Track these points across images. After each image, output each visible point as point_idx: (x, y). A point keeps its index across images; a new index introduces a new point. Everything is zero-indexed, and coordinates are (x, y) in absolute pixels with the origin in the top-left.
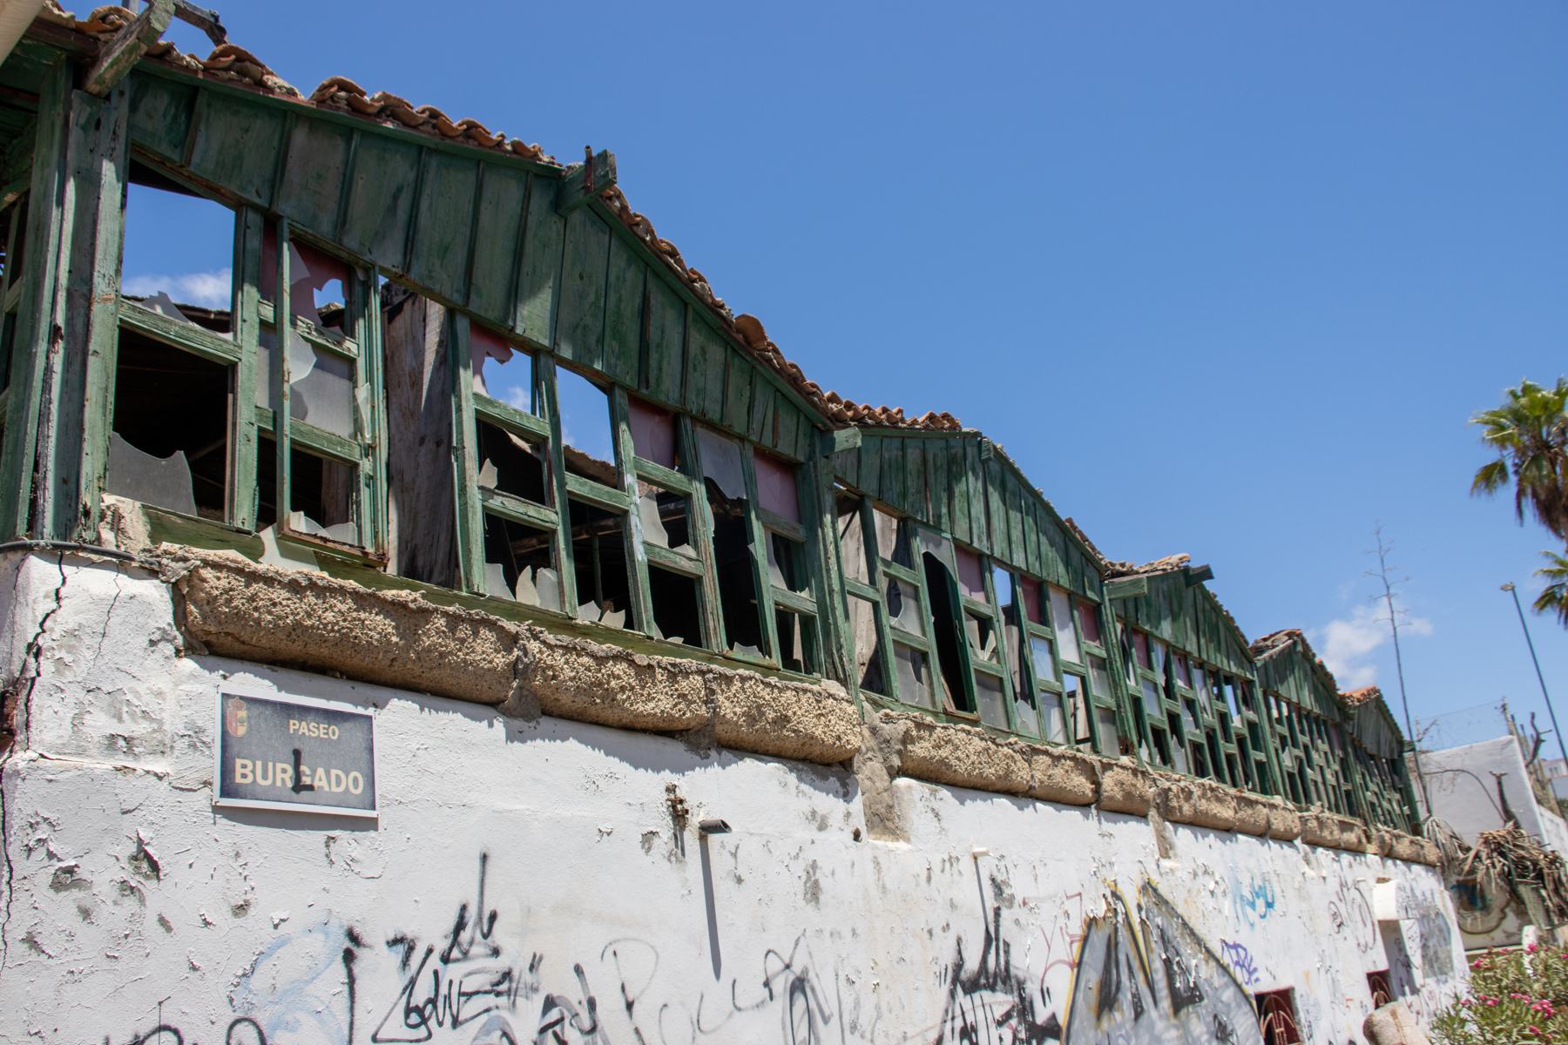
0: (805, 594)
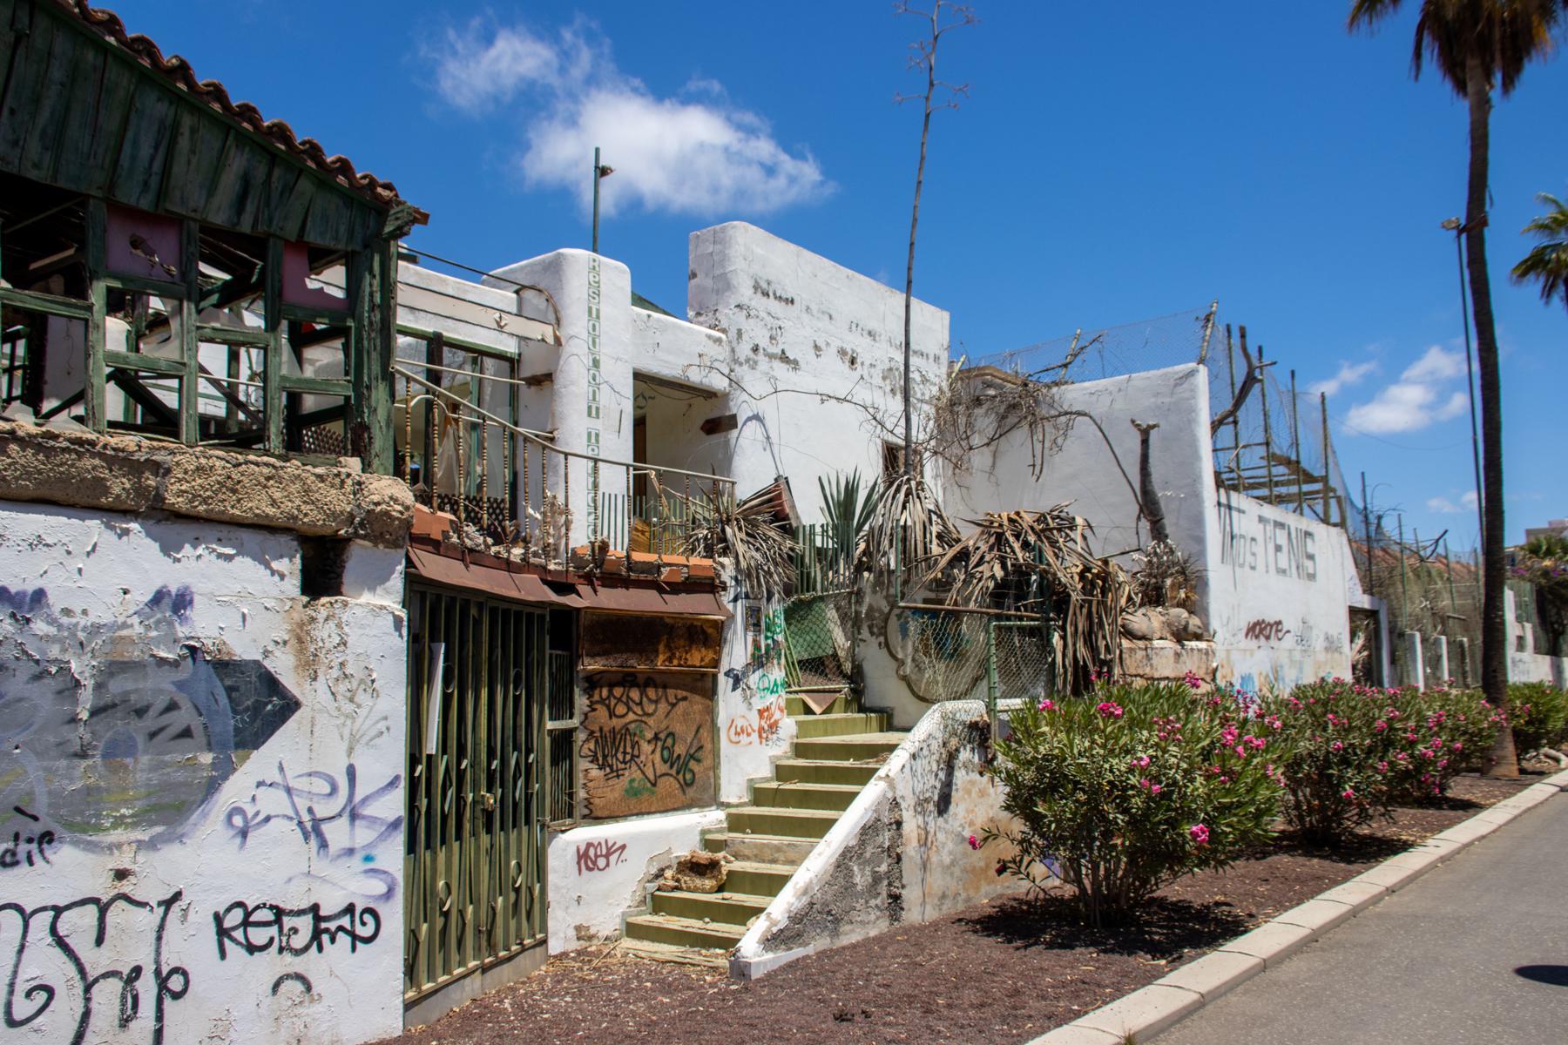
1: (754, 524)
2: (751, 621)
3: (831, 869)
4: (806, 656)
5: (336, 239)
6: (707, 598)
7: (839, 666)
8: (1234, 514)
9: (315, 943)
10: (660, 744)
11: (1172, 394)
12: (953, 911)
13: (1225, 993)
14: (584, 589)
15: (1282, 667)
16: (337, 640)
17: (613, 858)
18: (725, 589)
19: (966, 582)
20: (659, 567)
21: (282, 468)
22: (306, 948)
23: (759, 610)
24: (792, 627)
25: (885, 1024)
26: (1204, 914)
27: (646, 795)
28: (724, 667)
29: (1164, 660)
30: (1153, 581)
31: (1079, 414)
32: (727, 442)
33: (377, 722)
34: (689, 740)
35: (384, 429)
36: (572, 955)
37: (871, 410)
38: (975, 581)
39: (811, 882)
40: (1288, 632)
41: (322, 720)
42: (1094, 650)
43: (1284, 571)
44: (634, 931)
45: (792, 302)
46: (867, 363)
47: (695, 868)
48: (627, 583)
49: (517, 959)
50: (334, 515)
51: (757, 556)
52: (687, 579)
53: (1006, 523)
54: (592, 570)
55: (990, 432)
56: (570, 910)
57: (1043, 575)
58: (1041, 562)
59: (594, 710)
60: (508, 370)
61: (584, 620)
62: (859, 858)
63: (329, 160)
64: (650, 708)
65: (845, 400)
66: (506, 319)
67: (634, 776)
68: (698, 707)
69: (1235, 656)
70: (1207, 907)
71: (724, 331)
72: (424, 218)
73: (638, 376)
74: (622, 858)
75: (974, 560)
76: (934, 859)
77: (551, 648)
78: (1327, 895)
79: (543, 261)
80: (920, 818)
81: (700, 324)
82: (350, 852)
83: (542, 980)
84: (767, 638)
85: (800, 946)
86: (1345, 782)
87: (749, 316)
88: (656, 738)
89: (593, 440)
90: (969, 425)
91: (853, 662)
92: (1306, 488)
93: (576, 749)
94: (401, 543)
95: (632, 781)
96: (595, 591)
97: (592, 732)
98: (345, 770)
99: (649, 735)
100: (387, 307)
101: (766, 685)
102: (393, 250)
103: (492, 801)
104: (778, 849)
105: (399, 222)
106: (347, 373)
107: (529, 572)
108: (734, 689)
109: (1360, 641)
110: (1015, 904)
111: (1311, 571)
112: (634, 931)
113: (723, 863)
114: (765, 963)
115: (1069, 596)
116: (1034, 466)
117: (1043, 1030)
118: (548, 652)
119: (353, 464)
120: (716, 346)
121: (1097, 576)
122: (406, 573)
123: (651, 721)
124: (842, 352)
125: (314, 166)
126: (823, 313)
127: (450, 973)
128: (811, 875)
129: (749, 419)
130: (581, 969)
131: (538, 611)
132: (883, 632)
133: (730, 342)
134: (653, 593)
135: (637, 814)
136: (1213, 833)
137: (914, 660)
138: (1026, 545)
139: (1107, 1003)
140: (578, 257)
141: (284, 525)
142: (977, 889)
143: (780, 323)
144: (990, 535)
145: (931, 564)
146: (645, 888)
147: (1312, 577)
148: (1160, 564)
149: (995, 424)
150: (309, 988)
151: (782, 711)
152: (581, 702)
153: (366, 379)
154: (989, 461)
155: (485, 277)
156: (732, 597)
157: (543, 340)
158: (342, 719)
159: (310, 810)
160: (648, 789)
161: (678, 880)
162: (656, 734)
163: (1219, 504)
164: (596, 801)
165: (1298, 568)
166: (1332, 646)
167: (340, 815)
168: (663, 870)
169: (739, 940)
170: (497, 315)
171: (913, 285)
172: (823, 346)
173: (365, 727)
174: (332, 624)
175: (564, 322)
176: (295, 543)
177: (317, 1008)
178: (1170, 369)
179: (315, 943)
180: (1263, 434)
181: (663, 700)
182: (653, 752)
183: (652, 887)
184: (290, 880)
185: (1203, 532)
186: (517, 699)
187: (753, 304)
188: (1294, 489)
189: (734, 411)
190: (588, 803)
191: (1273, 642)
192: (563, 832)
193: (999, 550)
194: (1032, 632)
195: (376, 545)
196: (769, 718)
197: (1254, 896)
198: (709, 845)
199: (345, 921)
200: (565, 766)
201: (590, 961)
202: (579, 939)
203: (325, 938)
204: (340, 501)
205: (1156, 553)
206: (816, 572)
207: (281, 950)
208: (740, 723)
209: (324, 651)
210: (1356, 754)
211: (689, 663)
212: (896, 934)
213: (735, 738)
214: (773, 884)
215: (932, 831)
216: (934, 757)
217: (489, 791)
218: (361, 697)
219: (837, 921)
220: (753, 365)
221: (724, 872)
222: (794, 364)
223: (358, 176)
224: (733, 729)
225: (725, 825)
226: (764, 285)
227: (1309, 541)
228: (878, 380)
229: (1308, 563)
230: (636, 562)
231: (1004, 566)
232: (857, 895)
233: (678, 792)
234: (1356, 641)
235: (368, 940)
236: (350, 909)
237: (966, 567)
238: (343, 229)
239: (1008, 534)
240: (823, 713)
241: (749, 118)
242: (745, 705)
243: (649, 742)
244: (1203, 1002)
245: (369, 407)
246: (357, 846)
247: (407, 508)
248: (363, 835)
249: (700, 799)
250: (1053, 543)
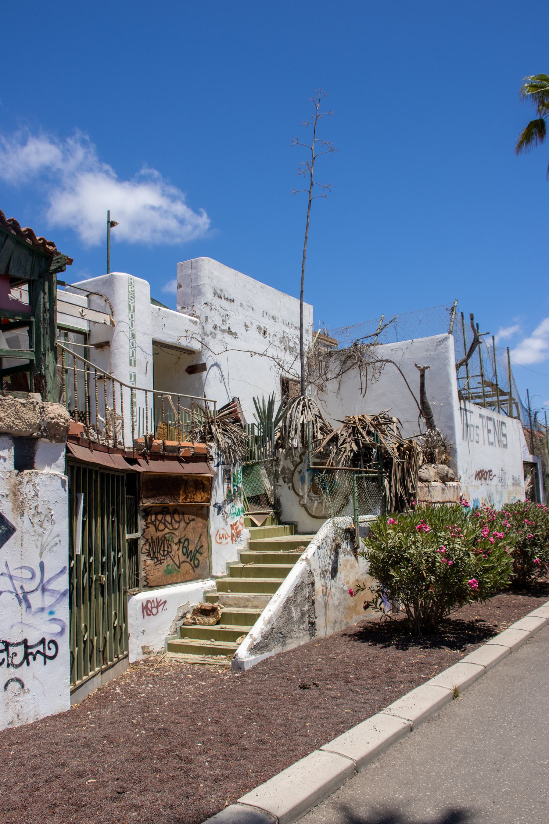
0: (32, 320)
1: (225, 423)
2: (226, 477)
3: (281, 609)
4: (251, 495)
5: (25, 273)
6: (204, 464)
7: (268, 500)
8: (468, 413)
9: (26, 661)
10: (181, 545)
11: (435, 350)
12: (340, 630)
13: (495, 666)
14: (142, 461)
15: (492, 494)
16: (33, 493)
17: (160, 608)
18: (212, 460)
19: (337, 454)
20: (179, 448)
21: (4, 400)
22: (21, 664)
23: (230, 471)
25: (327, 689)
26: (471, 626)
27: (175, 573)
28: (213, 502)
29: (437, 493)
30: (429, 450)
31: (387, 361)
32: (201, 378)
33: (54, 538)
34: (196, 542)
35: (53, 377)
36: (142, 662)
37: (277, 360)
38: (342, 453)
39: (272, 616)
40: (495, 475)
41: (26, 537)
42: (405, 488)
43: (492, 443)
44: (172, 648)
45: (233, 301)
46: (272, 334)
47: (203, 612)
48: (162, 458)
49: (116, 666)
50: (31, 425)
51: (230, 441)
52: (193, 454)
53: (357, 421)
54: (145, 451)
55: (337, 371)
56: (139, 638)
57: (379, 449)
58: (377, 442)
59: (148, 527)
60: (83, 339)
61: (142, 479)
62: (294, 603)
63: (23, 229)
64: (176, 526)
65: (263, 355)
66: (86, 312)
67: (169, 563)
68: (200, 524)
69: (470, 489)
70: (472, 622)
71: (198, 317)
72: (70, 261)
73: (155, 343)
74: (165, 608)
75: (340, 442)
76: (330, 602)
77: (127, 495)
78: (532, 614)
79: (103, 279)
80: (323, 580)
81: (185, 313)
82: (42, 609)
83: (131, 677)
84: (234, 486)
85: (267, 651)
86: (534, 555)
87: (211, 309)
88: (180, 542)
89: (133, 378)
90: (327, 367)
91: (275, 497)
92: (501, 398)
93: (139, 549)
94: (64, 439)
95: (168, 565)
96: (148, 462)
97: (147, 540)
98: (39, 565)
99: (176, 540)
100: (52, 311)
101: (235, 511)
102: (54, 279)
103: (104, 579)
104: (248, 600)
105: (59, 264)
106: (31, 347)
107: (117, 454)
108: (218, 514)
109: (529, 480)
110: (370, 625)
111: (505, 443)
112: (172, 648)
113: (219, 608)
114: (251, 661)
115: (392, 459)
116: (362, 389)
117: (411, 689)
118: (126, 496)
119: (37, 397)
120: (194, 326)
121: (407, 449)
122: (66, 456)
123: (177, 533)
124: (259, 328)
125: (15, 233)
126: (249, 307)
127: (87, 675)
128: (271, 613)
129: (213, 365)
130: (149, 670)
131: (121, 474)
132: (291, 481)
133: (201, 323)
134: (176, 463)
135: (171, 584)
136: (480, 582)
137: (308, 496)
138: (369, 433)
139: (438, 673)
140: (122, 277)
141: (5, 431)
142: (351, 618)
143: (227, 313)
144: (348, 428)
145: (317, 443)
146: (176, 624)
147: (505, 446)
148: (433, 441)
149: (340, 367)
150: (23, 686)
151: (242, 525)
152: (141, 523)
153: (42, 350)
154: (337, 386)
155: (68, 287)
156: (216, 464)
157: (105, 323)
158: (37, 537)
159: (22, 588)
160: (176, 570)
161: (194, 619)
162: (179, 540)
163: (461, 408)
164: (150, 577)
165: (499, 441)
166: (516, 483)
167: (37, 589)
168: (185, 614)
169: (236, 650)
170: (80, 309)
171: (304, 293)
172: (249, 325)
173: (48, 541)
174: (30, 485)
175: (116, 313)
176: (11, 441)
177: (28, 697)
178: (434, 337)
179: (26, 661)
180: (480, 370)
181: (183, 521)
182: (178, 549)
183: (180, 623)
184: (12, 626)
185: (453, 423)
186: (113, 522)
187: (213, 302)
188: (495, 399)
190: (146, 579)
191: (488, 481)
192: (134, 595)
193: (354, 436)
194: (374, 479)
195: (51, 441)
196: (236, 529)
197: (495, 616)
198: (208, 599)
199: (40, 648)
200: (134, 558)
201: (152, 665)
202: (144, 653)
203: (31, 657)
204: (33, 417)
205: (430, 435)
206: (255, 449)
207: (8, 665)
208: (222, 532)
209: (27, 500)
210: (539, 540)
211: (195, 500)
212: (314, 643)
213: (219, 541)
214: (251, 619)
215: (329, 587)
216: (329, 548)
217: (102, 574)
218: (46, 524)
219: (285, 637)
220: (214, 336)
221: (220, 614)
222: (234, 335)
223: (38, 238)
225: (216, 588)
226: (219, 292)
227: (503, 427)
228: (277, 343)
229: (503, 439)
230: (168, 446)
231: (357, 444)
232: (294, 623)
233: (191, 571)
234: (527, 479)
235: (52, 658)
236: (43, 641)
237: (337, 445)
238: (28, 268)
239: (359, 427)
240: (262, 525)
241: (173, 190)
242: (224, 523)
243: (176, 544)
244: (486, 670)
245: (45, 365)
246: (46, 606)
247: (67, 421)
248: (49, 600)
249: (202, 575)
250: (383, 432)
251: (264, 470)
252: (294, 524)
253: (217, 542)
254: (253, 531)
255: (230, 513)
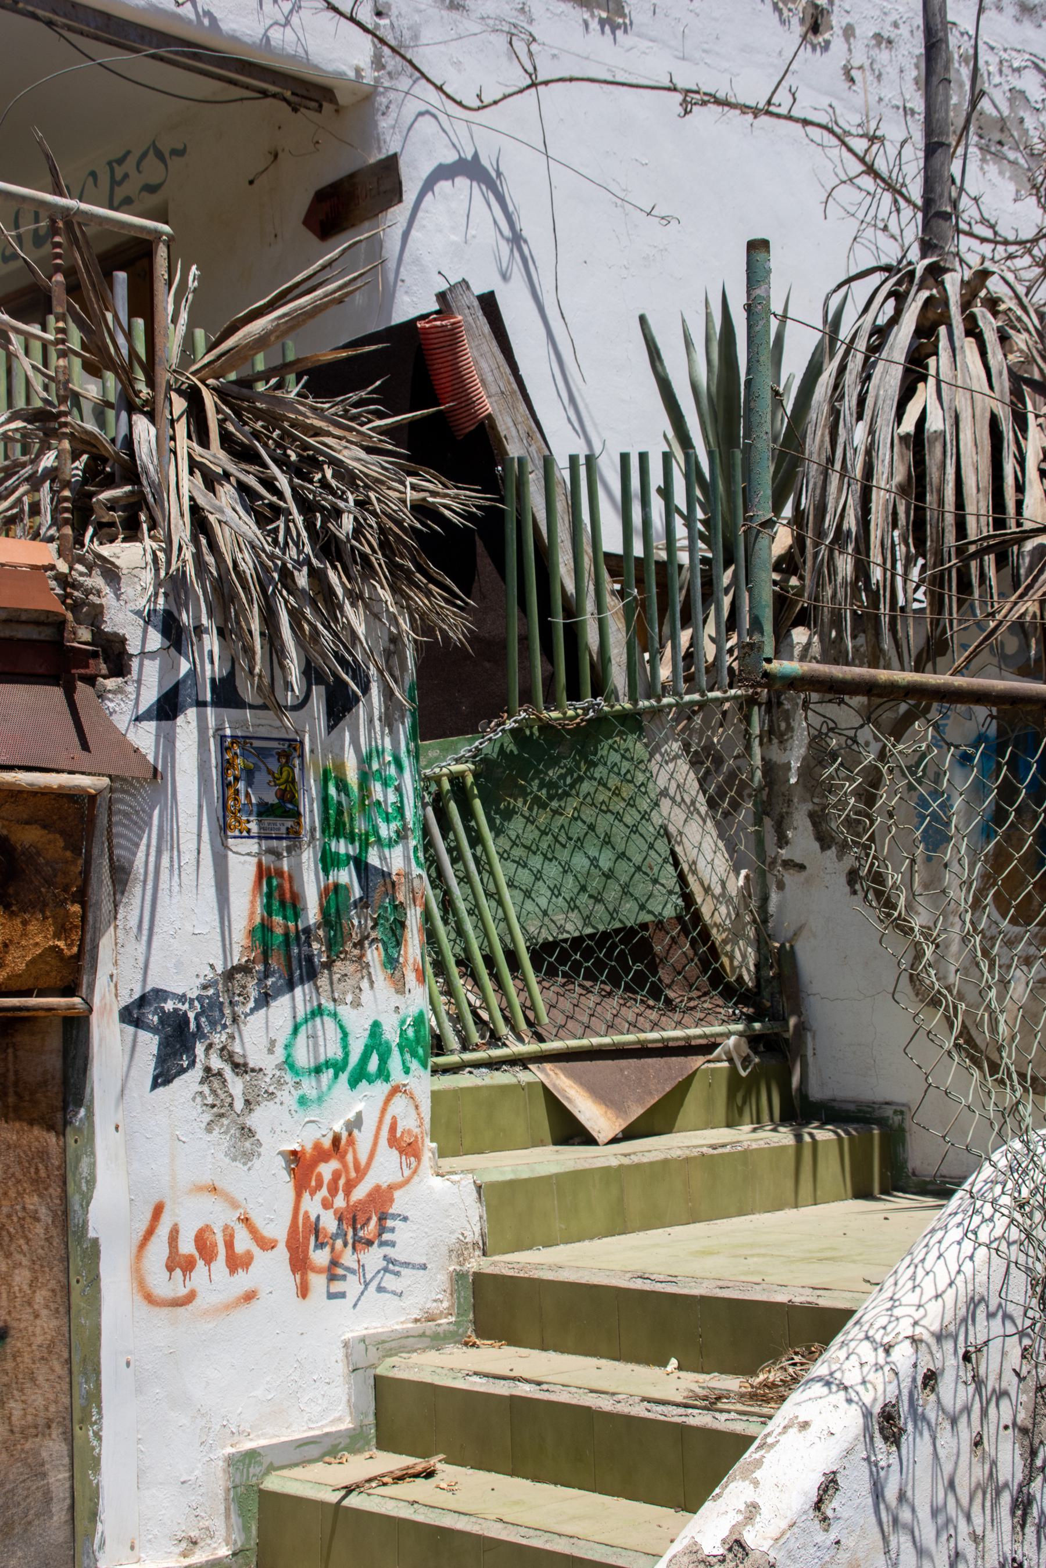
2: (248, 794)
4: (572, 927)
24: (516, 826)
32: (376, 245)
46: (865, 31)
84: (328, 861)
91: (761, 943)
101: (332, 1050)
108: (162, 1078)
129: (443, 173)
151: (409, 1149)
156: (150, 696)
189: (392, 146)
213: (164, 1285)
224: (158, 1250)
240: (629, 1134)
242: (220, 1140)
251: (683, 766)
252: (882, 1122)
253: (150, 1299)
254: (513, 1185)
255: (289, 1064)
